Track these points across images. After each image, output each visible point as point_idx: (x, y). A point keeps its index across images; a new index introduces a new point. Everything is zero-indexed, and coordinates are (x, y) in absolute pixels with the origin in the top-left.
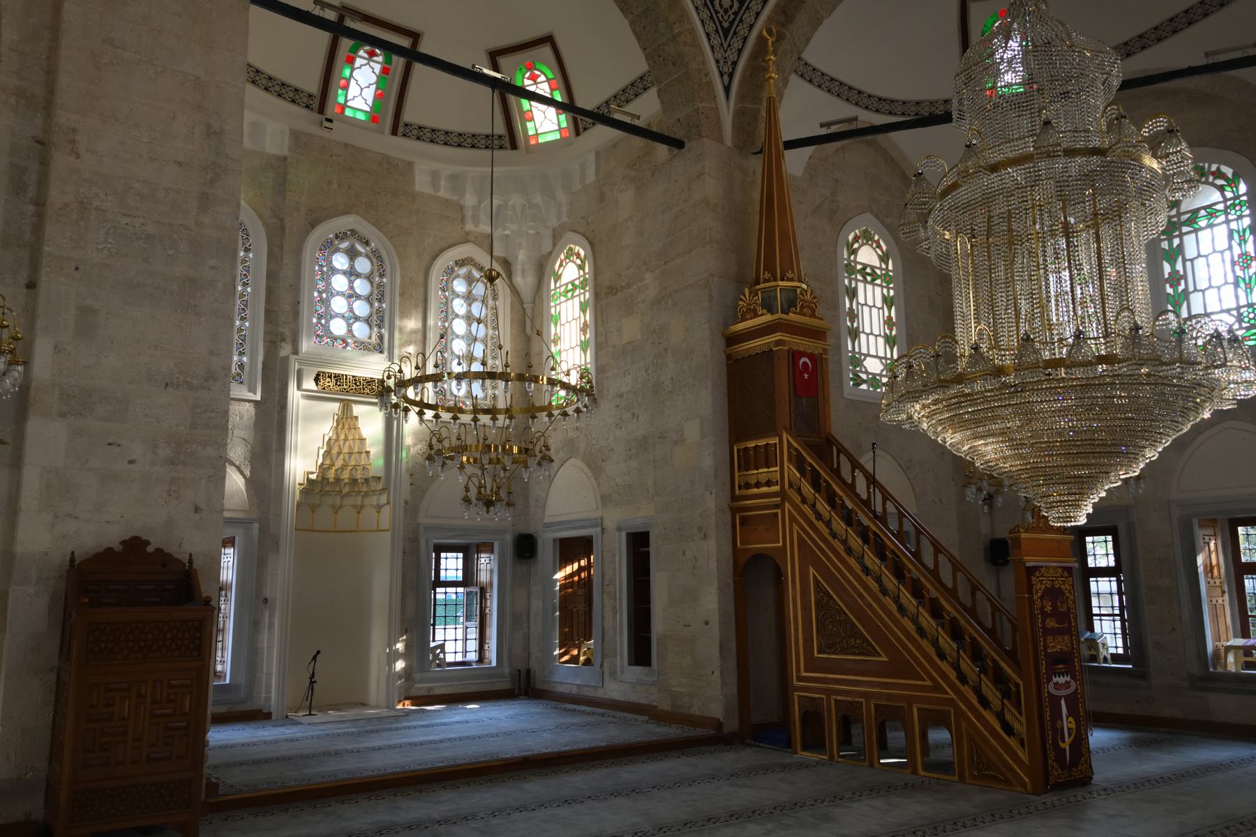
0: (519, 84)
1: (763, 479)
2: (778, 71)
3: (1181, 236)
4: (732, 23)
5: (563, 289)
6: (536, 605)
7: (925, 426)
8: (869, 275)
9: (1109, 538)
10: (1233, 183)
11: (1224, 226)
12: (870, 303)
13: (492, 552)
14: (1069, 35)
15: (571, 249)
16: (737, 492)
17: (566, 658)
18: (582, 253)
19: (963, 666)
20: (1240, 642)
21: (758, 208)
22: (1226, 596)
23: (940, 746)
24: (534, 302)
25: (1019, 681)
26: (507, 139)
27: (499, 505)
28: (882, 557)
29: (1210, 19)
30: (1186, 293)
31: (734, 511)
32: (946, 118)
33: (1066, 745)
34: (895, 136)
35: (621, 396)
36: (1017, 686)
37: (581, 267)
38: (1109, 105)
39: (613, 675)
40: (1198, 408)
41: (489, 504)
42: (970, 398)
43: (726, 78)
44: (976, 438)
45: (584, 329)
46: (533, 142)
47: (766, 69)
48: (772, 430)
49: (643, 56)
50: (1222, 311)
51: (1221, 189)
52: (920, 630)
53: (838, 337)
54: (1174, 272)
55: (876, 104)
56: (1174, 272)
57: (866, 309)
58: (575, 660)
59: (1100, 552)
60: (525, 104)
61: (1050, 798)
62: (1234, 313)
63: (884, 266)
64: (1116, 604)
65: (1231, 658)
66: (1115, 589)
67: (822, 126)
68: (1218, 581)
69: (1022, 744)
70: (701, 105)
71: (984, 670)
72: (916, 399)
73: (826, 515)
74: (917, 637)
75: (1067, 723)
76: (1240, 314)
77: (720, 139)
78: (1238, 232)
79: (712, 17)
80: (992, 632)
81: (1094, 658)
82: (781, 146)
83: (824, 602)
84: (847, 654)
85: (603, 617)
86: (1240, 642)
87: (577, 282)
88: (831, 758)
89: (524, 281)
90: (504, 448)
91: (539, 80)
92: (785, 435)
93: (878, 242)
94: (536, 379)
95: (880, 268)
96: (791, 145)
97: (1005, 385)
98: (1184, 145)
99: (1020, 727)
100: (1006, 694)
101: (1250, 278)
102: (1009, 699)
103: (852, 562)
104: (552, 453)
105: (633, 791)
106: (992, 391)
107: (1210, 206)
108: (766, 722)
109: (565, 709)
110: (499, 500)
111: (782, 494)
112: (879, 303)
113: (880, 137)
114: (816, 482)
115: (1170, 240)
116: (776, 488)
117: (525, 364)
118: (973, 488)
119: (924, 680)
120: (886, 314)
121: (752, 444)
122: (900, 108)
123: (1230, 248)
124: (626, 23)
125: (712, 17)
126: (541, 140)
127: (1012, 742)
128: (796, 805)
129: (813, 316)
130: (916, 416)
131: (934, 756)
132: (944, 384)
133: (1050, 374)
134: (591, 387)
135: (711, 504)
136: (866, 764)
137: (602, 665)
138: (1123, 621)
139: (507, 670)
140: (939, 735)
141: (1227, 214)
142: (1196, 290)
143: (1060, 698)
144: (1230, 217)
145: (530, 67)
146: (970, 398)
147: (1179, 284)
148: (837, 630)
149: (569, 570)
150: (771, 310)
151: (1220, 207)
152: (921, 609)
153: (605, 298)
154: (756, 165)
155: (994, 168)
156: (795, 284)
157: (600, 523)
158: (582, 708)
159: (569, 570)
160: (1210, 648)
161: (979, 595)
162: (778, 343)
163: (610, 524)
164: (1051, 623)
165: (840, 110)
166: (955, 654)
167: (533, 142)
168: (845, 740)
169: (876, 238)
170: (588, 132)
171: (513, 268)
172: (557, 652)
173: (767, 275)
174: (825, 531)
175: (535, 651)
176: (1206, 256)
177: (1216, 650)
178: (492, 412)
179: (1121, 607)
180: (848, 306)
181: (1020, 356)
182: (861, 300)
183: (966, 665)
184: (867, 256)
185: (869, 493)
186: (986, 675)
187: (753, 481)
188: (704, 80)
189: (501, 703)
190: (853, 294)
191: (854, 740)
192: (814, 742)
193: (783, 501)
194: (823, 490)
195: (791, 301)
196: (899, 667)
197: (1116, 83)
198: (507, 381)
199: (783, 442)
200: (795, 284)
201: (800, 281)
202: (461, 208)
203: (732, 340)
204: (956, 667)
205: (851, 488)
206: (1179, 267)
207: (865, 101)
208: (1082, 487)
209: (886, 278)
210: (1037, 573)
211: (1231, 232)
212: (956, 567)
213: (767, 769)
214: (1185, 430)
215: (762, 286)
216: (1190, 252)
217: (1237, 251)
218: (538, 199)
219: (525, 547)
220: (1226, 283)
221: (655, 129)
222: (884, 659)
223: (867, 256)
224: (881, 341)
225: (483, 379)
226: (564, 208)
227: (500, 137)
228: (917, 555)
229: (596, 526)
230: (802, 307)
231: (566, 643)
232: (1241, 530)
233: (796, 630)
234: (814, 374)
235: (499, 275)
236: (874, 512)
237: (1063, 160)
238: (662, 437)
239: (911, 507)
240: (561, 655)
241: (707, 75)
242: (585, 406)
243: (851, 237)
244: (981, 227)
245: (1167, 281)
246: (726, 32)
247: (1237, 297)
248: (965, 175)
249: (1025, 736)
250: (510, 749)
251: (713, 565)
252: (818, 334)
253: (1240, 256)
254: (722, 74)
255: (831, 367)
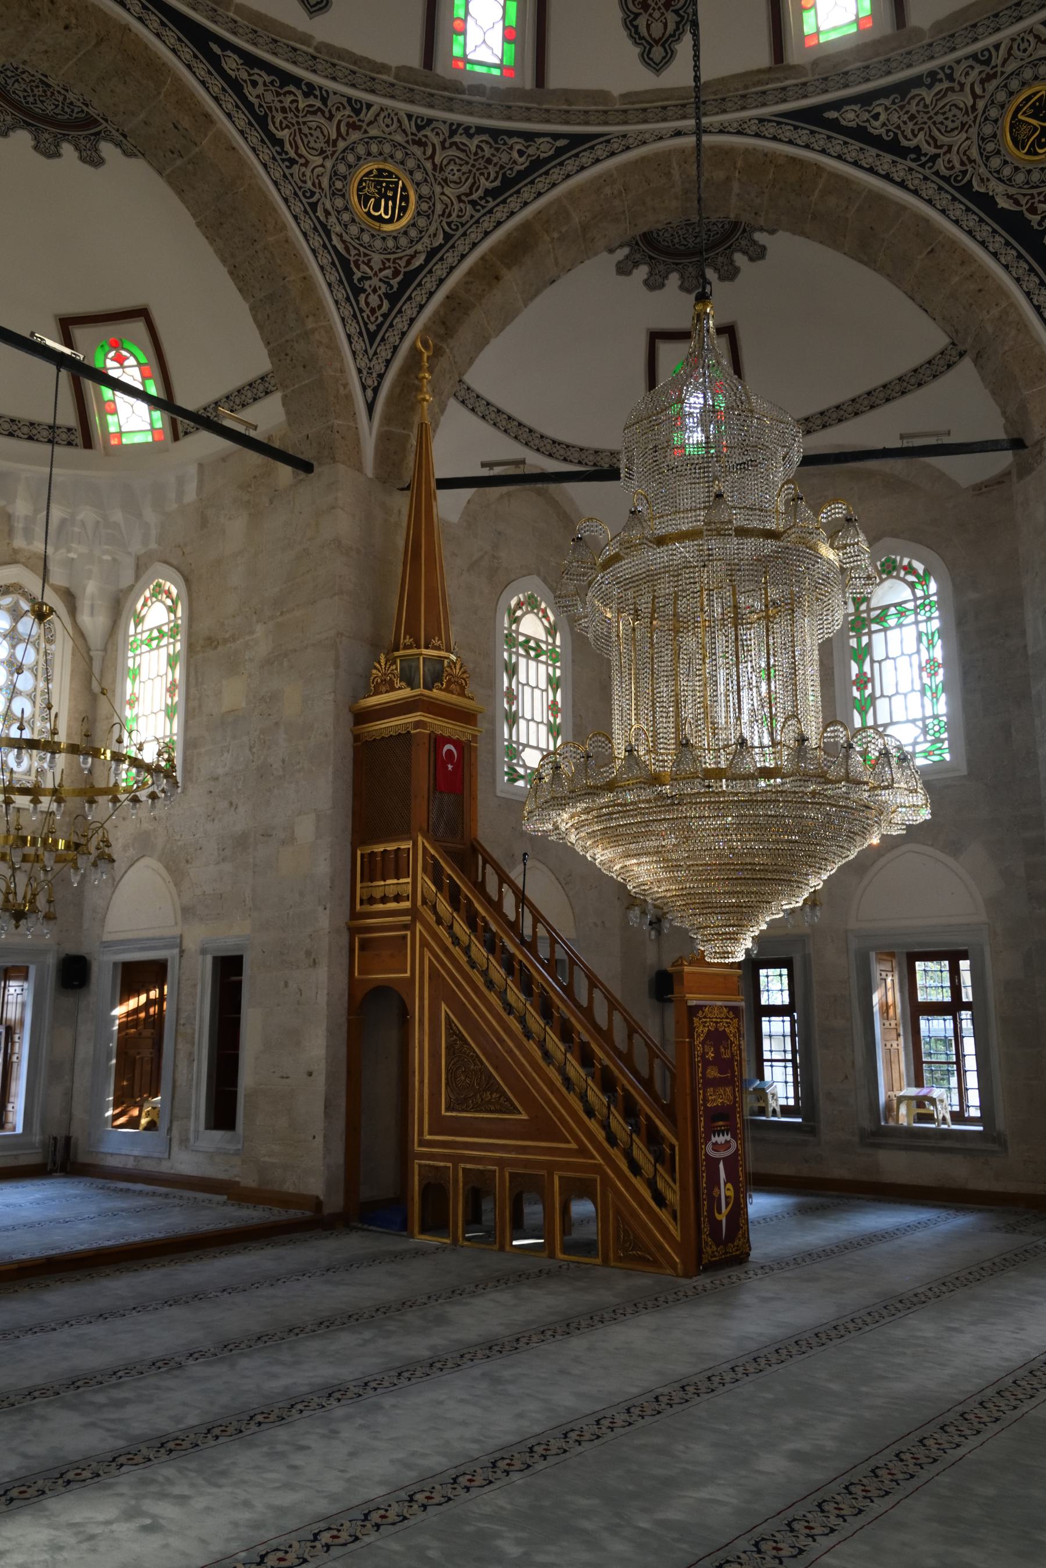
0: (98, 365)
1: (391, 892)
2: (434, 393)
3: (870, 634)
4: (379, 327)
5: (146, 635)
6: (85, 1050)
7: (573, 838)
8: (532, 649)
9: (785, 971)
10: (923, 581)
11: (914, 626)
12: (533, 683)
13: (26, 978)
14: (748, 398)
15: (159, 585)
16: (358, 907)
17: (122, 1120)
18: (174, 591)
19: (613, 1124)
20: (913, 1091)
21: (402, 557)
22: (901, 1039)
23: (584, 1221)
24: (105, 650)
25: (674, 1141)
26: (79, 433)
27: (32, 918)
28: (528, 991)
29: (908, 397)
30: (873, 698)
31: (353, 931)
32: (611, 474)
33: (722, 1218)
34: (573, 488)
35: (217, 779)
36: (672, 1147)
37: (171, 610)
38: (786, 483)
39: (184, 1142)
40: (865, 832)
41: (19, 916)
42: (625, 810)
43: (370, 393)
44: (628, 856)
45: (171, 690)
46: (114, 442)
47: (419, 389)
48: (404, 831)
49: (266, 352)
50: (908, 721)
51: (912, 586)
52: (567, 1081)
53: (492, 721)
54: (861, 674)
55: (549, 447)
56: (861, 674)
57: (527, 689)
58: (133, 1123)
59: (774, 986)
60: (107, 393)
61: (703, 1281)
62: (920, 724)
63: (550, 640)
64: (789, 1047)
65: (903, 1110)
66: (788, 1030)
67: (484, 465)
68: (893, 1023)
69: (675, 1218)
70: (337, 422)
71: (636, 1129)
72: (562, 807)
73: (464, 939)
74: (563, 1090)
75: (725, 1190)
76: (925, 726)
77: (359, 468)
78: (927, 634)
79: (355, 316)
80: (648, 1084)
81: (762, 1111)
82: (433, 484)
83: (457, 1047)
84: (480, 1111)
85: (175, 1066)
86: (913, 1091)
87: (165, 629)
88: (455, 1241)
89: (93, 622)
90: (45, 842)
91: (126, 363)
92: (420, 839)
93: (544, 611)
94: (96, 753)
95: (546, 643)
96: (445, 484)
97: (661, 796)
98: (862, 537)
99: (673, 1197)
100: (659, 1158)
101: (937, 686)
102: (663, 1163)
103: (492, 997)
104: (116, 851)
105: (197, 1296)
106: (648, 801)
107: (900, 604)
108: (380, 1199)
109: (115, 1190)
110: (34, 910)
111: (413, 912)
112: (543, 684)
113: (552, 487)
114: (455, 898)
115: (859, 637)
116: (406, 905)
117: (92, 730)
118: (637, 911)
119: (569, 1142)
120: (551, 698)
121: (379, 848)
122: (575, 456)
123: (918, 652)
124: (245, 307)
125: (355, 316)
126: (126, 440)
127: (664, 1215)
128: (405, 1305)
129: (462, 694)
130: (563, 827)
131: (576, 1235)
132: (593, 792)
133: (709, 787)
134: (173, 767)
135: (324, 921)
136: (496, 1247)
137: (170, 1130)
138: (795, 1068)
139: (37, 1138)
140: (582, 1208)
141: (917, 614)
142: (882, 696)
143: (718, 1160)
144: (920, 618)
145: (116, 345)
146: (625, 810)
147: (866, 687)
148: (472, 1082)
149: (133, 1003)
150: (411, 684)
151: (910, 605)
152: (569, 1056)
153: (203, 651)
154: (402, 503)
155: (661, 541)
156: (443, 654)
157: (179, 943)
158: (139, 1187)
159: (133, 1003)
160: (882, 1099)
161: (637, 1039)
162: (418, 724)
163: (191, 945)
164: (713, 1073)
165: (507, 449)
166: (605, 1111)
167: (114, 442)
168: (474, 1217)
169: (543, 606)
170: (189, 439)
171: (78, 604)
172: (110, 1113)
173: (408, 641)
174: (463, 959)
175: (78, 1113)
176: (894, 659)
177: (889, 1101)
178: (34, 792)
179: (794, 1051)
180: (506, 684)
181: (677, 763)
182: (522, 679)
183: (618, 1123)
184: (531, 626)
185: (517, 912)
186: (638, 1135)
187: (378, 894)
188: (342, 391)
189: (37, 1182)
190: (512, 670)
191: (484, 1218)
192: (435, 1221)
193: (414, 921)
194: (463, 909)
195: (437, 675)
196: (541, 1127)
197: (797, 459)
198: (53, 753)
199: (418, 847)
200: (443, 654)
201: (448, 650)
202: (9, 517)
203: (361, 717)
204: (606, 1126)
205: (496, 907)
206: (867, 668)
207: (537, 441)
208: (740, 915)
209: (553, 655)
210: (700, 1014)
211: (920, 635)
212: (613, 1005)
213: (374, 1259)
214: (852, 857)
215: (401, 653)
216: (878, 653)
217: (925, 655)
218: (118, 516)
219: (74, 973)
220: (913, 690)
221: (277, 445)
222: (524, 1116)
223: (531, 626)
224: (543, 729)
225: (20, 748)
226: (154, 533)
227: (69, 430)
228: (568, 990)
229: (172, 947)
230: (449, 682)
231: (124, 1098)
232: (919, 966)
233: (422, 1082)
234: (460, 765)
235: (52, 611)
236: (521, 936)
237: (735, 541)
238: (267, 835)
239: (566, 929)
240: (116, 1117)
241: (345, 386)
242: (163, 791)
243: (513, 602)
244: (645, 608)
245: (854, 683)
246: (372, 336)
247: (923, 706)
248: (629, 546)
249: (678, 1208)
250: (30, 1246)
251: (322, 999)
252: (467, 717)
253: (928, 662)
254: (364, 388)
255: (482, 756)
